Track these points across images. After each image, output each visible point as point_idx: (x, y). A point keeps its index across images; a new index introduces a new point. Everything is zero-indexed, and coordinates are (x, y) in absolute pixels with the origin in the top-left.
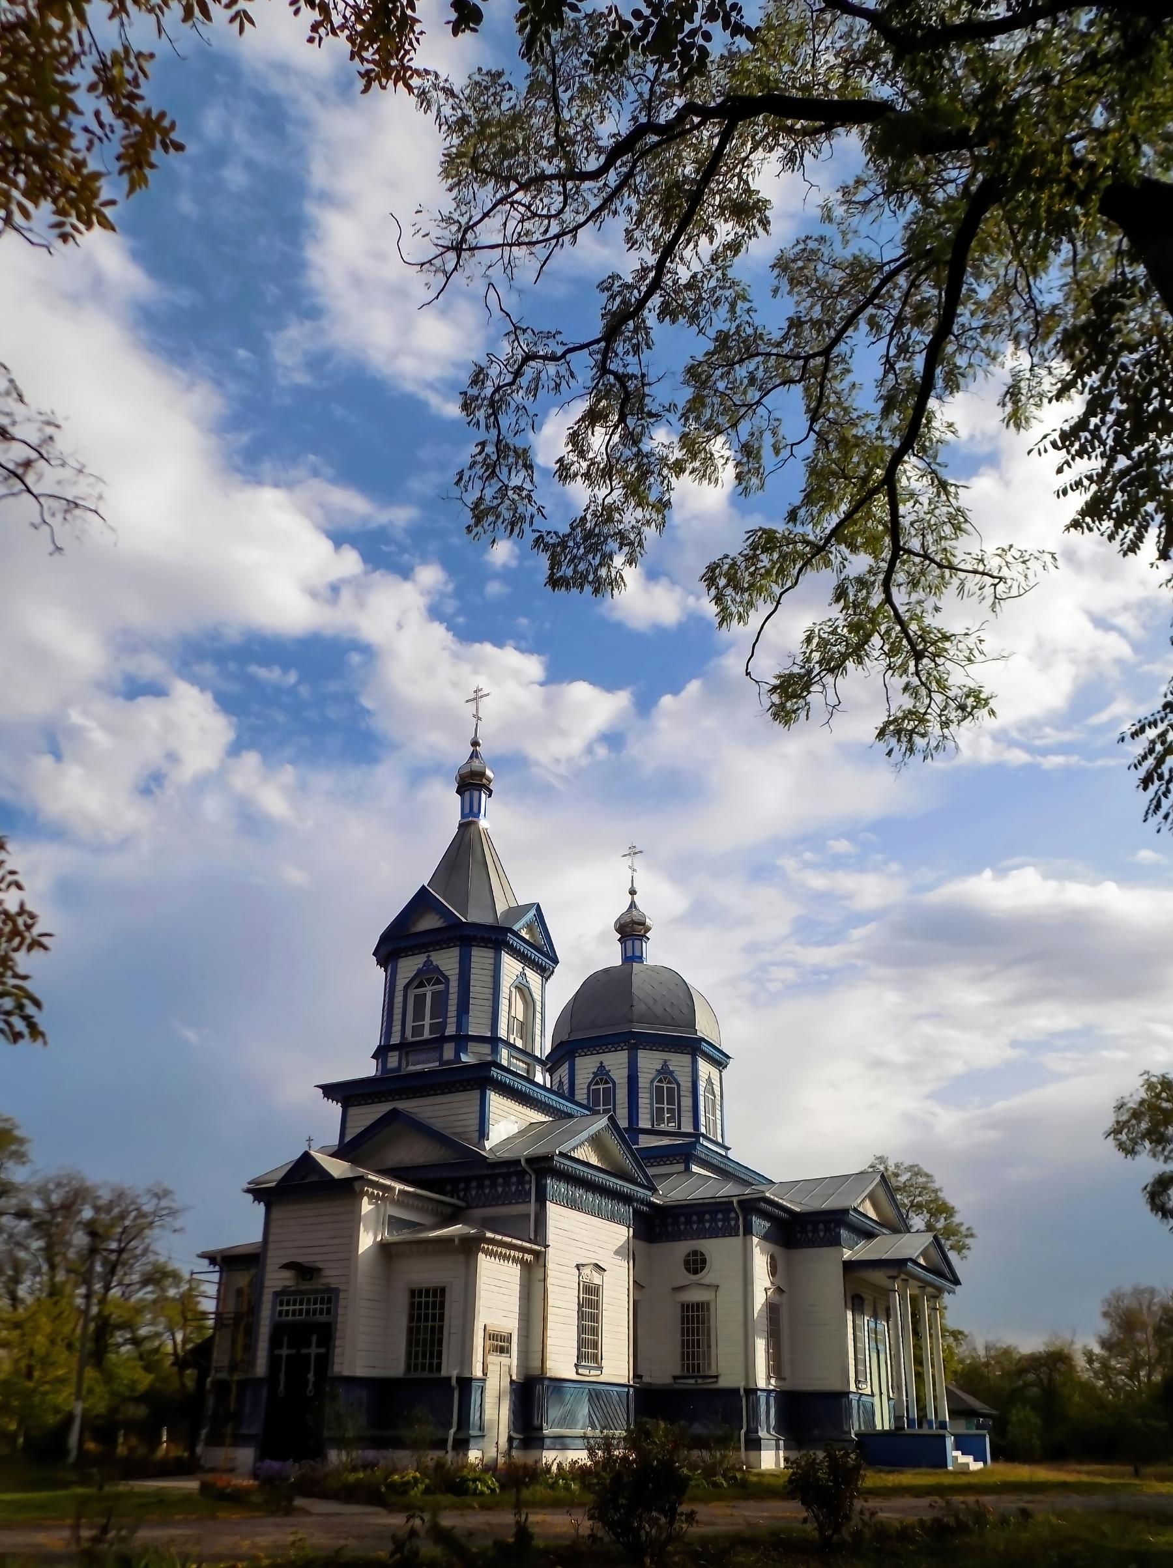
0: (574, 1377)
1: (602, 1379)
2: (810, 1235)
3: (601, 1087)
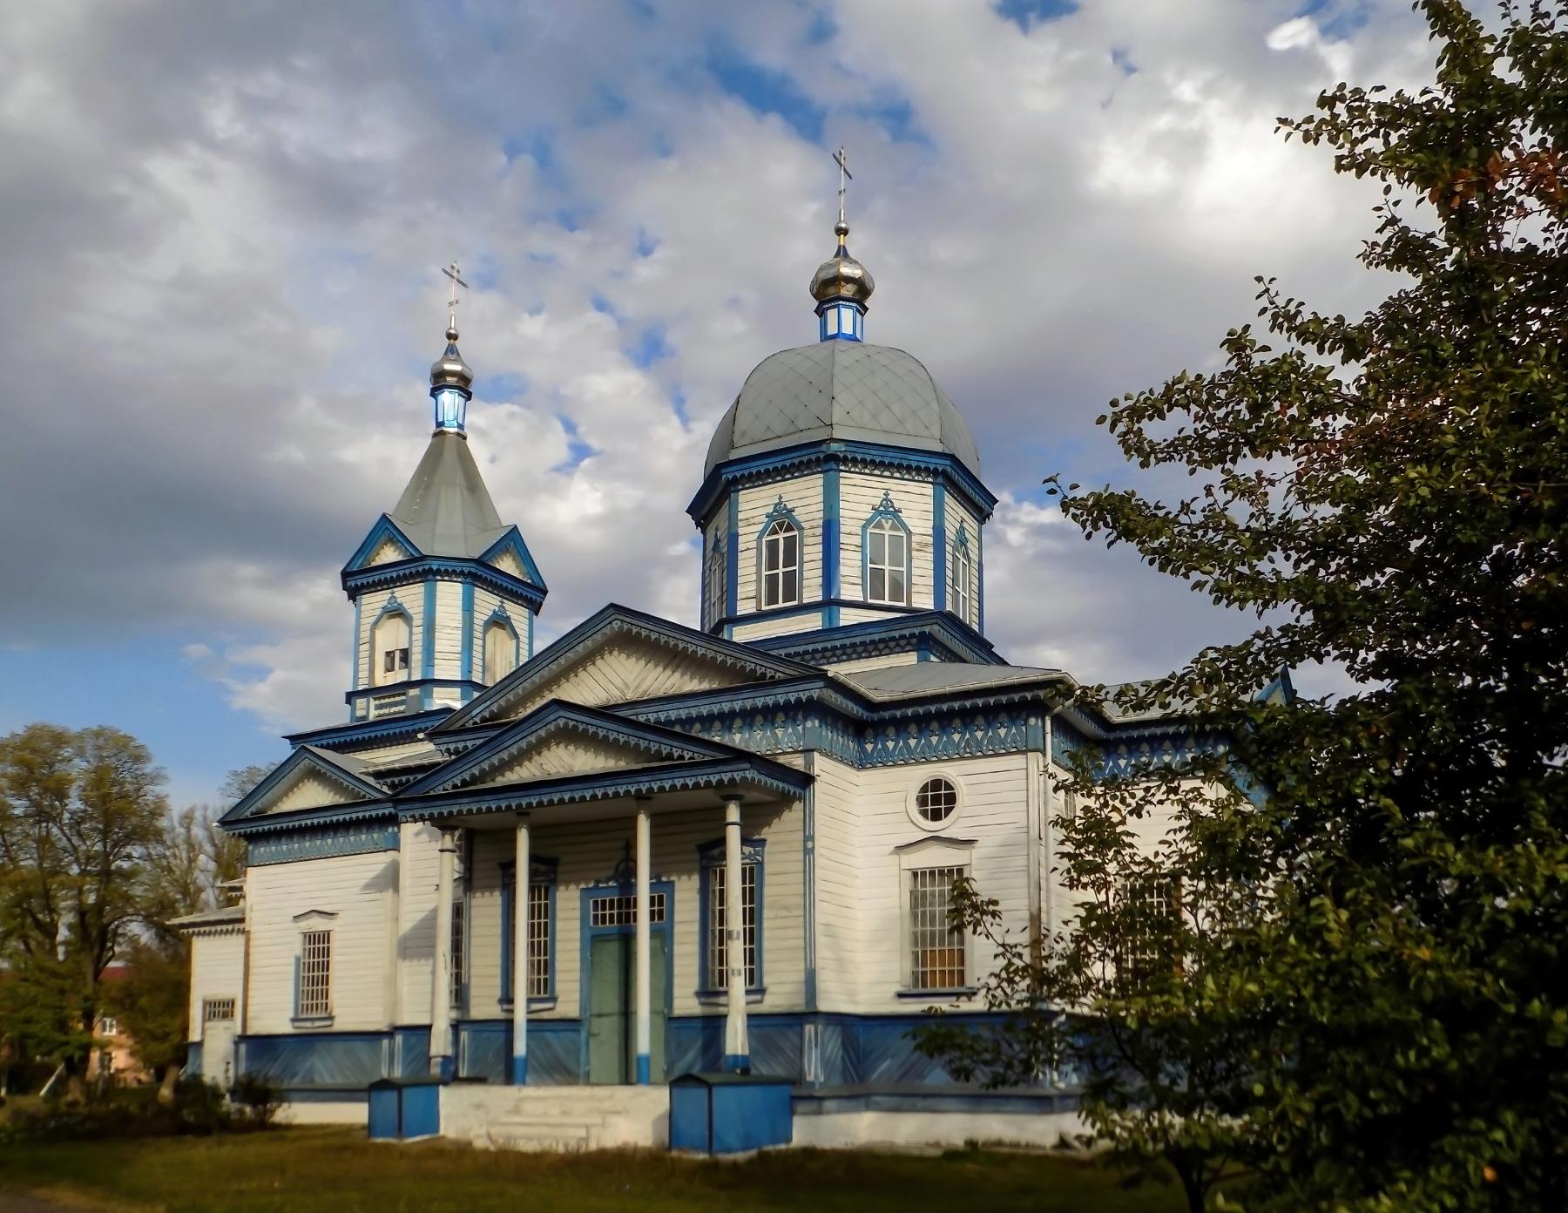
3: (781, 536)
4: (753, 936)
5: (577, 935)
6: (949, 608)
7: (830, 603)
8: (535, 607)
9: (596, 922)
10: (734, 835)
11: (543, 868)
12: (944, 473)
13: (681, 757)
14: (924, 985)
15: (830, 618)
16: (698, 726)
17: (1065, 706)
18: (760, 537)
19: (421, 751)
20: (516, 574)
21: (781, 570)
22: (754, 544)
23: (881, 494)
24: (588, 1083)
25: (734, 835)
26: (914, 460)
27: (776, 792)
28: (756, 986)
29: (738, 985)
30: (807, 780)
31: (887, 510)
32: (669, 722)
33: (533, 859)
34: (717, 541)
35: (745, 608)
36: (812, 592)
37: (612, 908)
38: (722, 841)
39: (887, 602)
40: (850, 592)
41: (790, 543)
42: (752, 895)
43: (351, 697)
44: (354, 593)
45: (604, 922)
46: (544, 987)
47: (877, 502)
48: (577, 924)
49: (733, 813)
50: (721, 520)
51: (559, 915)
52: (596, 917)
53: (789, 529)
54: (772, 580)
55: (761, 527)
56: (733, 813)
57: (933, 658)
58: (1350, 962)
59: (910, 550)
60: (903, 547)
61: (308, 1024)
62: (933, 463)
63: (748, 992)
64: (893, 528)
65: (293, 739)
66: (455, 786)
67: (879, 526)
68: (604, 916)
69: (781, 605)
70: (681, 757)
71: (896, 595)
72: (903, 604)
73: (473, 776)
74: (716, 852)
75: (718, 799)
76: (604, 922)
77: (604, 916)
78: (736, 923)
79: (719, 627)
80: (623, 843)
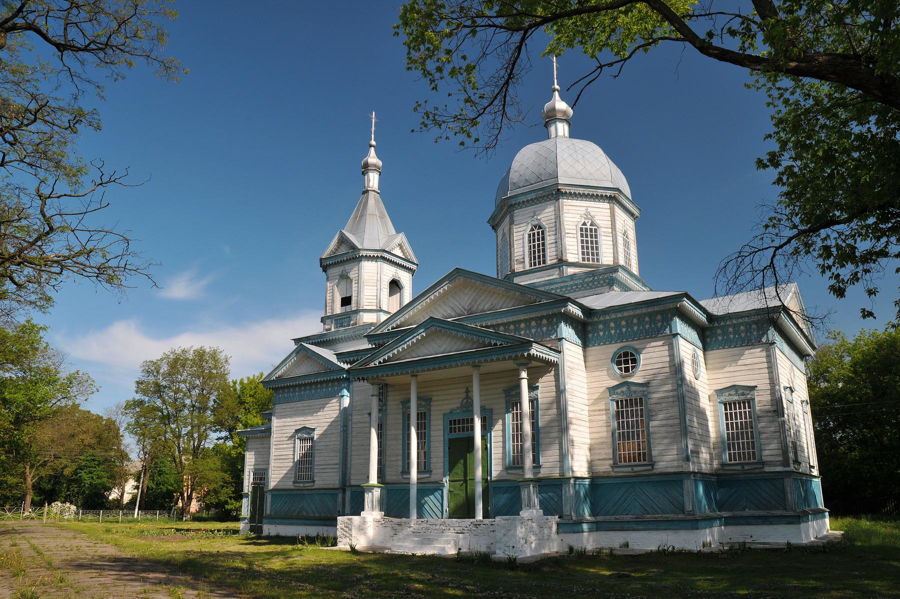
0: (292, 487)
1: (315, 487)
7: (561, 262)
10: (524, 384)
13: (496, 344)
14: (639, 460)
15: (561, 272)
16: (502, 328)
23: (584, 209)
24: (267, 470)
25: (524, 384)
26: (600, 192)
33: (419, 398)
34: (504, 235)
36: (550, 260)
38: (518, 387)
40: (571, 258)
44: (769, 154)
45: (463, 431)
46: (423, 468)
49: (524, 374)
56: (524, 374)
57: (615, 288)
62: (608, 193)
65: (297, 341)
66: (380, 363)
70: (496, 344)
73: (389, 357)
74: (514, 393)
80: (464, 390)
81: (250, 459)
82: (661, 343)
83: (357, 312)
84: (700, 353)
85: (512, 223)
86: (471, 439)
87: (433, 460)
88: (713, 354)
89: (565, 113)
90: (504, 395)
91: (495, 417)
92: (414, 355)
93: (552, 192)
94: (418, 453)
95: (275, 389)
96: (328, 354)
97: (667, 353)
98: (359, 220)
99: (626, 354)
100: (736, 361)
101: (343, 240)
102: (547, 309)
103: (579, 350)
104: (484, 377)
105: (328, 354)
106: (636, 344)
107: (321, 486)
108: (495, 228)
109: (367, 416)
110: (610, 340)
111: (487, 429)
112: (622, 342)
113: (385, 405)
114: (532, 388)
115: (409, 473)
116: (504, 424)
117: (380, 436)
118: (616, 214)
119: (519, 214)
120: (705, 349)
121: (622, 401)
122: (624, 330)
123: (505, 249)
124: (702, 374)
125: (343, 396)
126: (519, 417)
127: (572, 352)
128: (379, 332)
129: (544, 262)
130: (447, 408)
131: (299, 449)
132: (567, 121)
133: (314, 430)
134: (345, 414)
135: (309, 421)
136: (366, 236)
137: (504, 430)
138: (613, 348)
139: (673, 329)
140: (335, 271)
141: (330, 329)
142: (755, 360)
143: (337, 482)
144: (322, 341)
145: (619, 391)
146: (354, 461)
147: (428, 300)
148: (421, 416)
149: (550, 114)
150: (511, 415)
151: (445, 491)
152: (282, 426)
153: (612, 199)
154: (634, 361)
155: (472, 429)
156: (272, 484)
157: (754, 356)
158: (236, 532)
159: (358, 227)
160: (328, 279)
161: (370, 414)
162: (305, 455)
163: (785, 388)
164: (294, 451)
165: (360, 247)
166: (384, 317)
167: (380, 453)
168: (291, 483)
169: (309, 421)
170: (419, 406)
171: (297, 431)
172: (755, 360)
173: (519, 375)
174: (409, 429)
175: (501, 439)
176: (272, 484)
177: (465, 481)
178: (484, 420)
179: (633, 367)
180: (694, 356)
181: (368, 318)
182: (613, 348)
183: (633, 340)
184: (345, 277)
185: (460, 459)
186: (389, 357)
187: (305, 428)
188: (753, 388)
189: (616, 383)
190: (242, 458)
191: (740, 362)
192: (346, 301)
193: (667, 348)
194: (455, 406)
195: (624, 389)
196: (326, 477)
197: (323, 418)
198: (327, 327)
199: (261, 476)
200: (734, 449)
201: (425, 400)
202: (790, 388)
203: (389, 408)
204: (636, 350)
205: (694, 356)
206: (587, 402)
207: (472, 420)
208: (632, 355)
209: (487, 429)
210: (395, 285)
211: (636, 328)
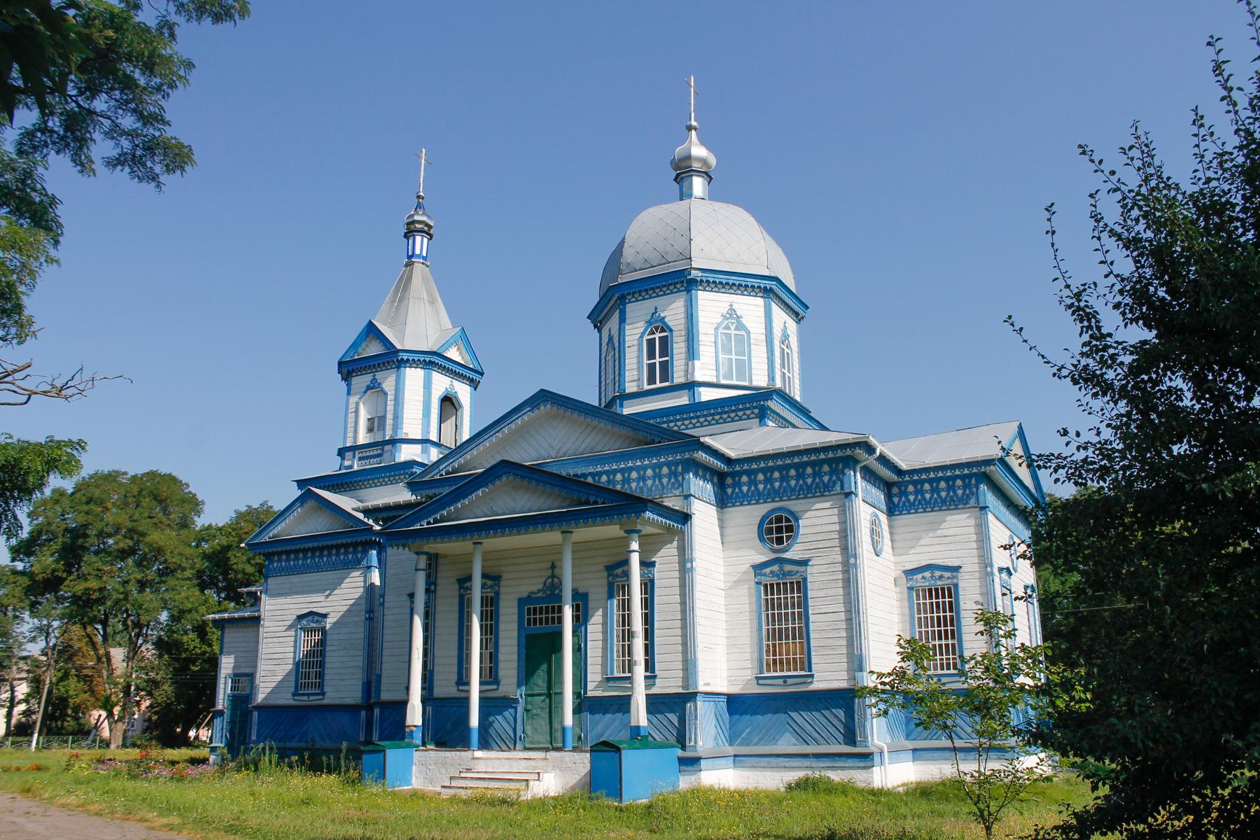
0: (291, 702)
1: (325, 702)
2: (793, 483)
3: (657, 336)
4: (649, 634)
5: (515, 634)
6: (779, 384)
8: (474, 384)
9: (529, 624)
10: (635, 559)
11: (489, 583)
12: (771, 290)
17: (871, 461)
18: (642, 337)
19: (402, 495)
20: (459, 359)
21: (658, 360)
22: (636, 343)
25: (635, 559)
26: (750, 281)
27: (661, 526)
28: (651, 678)
29: (640, 671)
30: (686, 518)
31: (732, 314)
32: (585, 475)
34: (611, 338)
35: (631, 388)
37: (541, 613)
38: (626, 562)
39: (735, 382)
41: (664, 341)
42: (648, 604)
43: (342, 452)
45: (541, 623)
46: (491, 675)
47: (725, 311)
48: (515, 626)
49: (635, 546)
50: (614, 322)
51: (502, 618)
52: (529, 620)
53: (663, 330)
54: (651, 368)
55: (641, 330)
56: (635, 546)
57: (770, 423)
58: (125, 537)
59: (749, 345)
60: (743, 341)
61: (305, 698)
62: (764, 283)
63: (646, 677)
64: (736, 329)
65: (301, 483)
67: (727, 327)
68: (535, 619)
69: (658, 385)
71: (741, 375)
72: (746, 384)
73: (442, 516)
74: (619, 571)
75: (622, 534)
76: (535, 623)
77: (535, 619)
78: (638, 625)
79: (611, 403)
81: (227, 665)
82: (827, 505)
83: (394, 442)
84: (883, 518)
85: (622, 320)
86: (559, 635)
87: (501, 665)
88: (903, 520)
89: (704, 161)
90: (605, 574)
91: (591, 604)
92: (478, 512)
93: (680, 280)
94: (481, 654)
95: (268, 556)
96: (345, 502)
97: (836, 519)
98: (398, 308)
99: (779, 519)
100: (934, 530)
101: (372, 331)
102: (670, 439)
103: (712, 511)
104: (579, 548)
105: (345, 502)
106: (794, 505)
107: (337, 702)
108: (598, 325)
109: (406, 598)
110: (758, 498)
111: (580, 620)
112: (773, 501)
113: (435, 584)
114: (646, 564)
115: (468, 683)
116: (605, 615)
117: (426, 628)
118: (774, 313)
119: (633, 309)
120: (891, 511)
121: (772, 585)
122: (777, 484)
123: (613, 353)
124: (885, 548)
125: (369, 567)
126: (626, 605)
127: (704, 514)
128: (426, 478)
129: (665, 375)
130: (524, 591)
131: (306, 643)
132: (707, 176)
133: (325, 616)
134: (372, 600)
135: (316, 602)
136: (409, 329)
137: (605, 624)
138: (759, 511)
139: (846, 486)
140: (361, 381)
141: (351, 467)
142: (959, 531)
143: (360, 694)
144: (339, 483)
145: (768, 570)
146: (388, 669)
147: (500, 435)
148: (485, 601)
149: (684, 164)
150: (615, 602)
151: (520, 709)
152: (279, 611)
153: (767, 292)
154: (790, 529)
155: (560, 620)
156: (260, 698)
157: (959, 523)
158: (204, 761)
159: (398, 317)
160: (349, 393)
161: (412, 596)
162: (309, 654)
163: (1001, 570)
164: (295, 647)
165: (399, 347)
166: (434, 455)
167: (425, 653)
168: (289, 695)
169: (316, 602)
170: (483, 586)
171: (300, 617)
172: (959, 531)
173: (628, 546)
174: (470, 620)
175: (600, 636)
176: (260, 698)
177: (549, 695)
178: (576, 608)
179: (788, 538)
180: (873, 523)
181: (406, 453)
182: (759, 511)
183: (789, 499)
184: (374, 386)
185: (542, 663)
186: (442, 516)
187: (311, 613)
188: (956, 569)
189: (763, 559)
190: (213, 663)
191: (939, 533)
192: (376, 423)
193: (836, 511)
194: (535, 588)
195: (776, 568)
196: (343, 687)
197: (340, 597)
198: (347, 463)
199: (245, 678)
200: (944, 597)
201: (492, 578)
202: (1008, 569)
203: (439, 588)
204: (792, 513)
205: (874, 522)
206: (722, 585)
207: (560, 610)
208: (788, 520)
209: (580, 620)
210: (449, 402)
211: (793, 483)
